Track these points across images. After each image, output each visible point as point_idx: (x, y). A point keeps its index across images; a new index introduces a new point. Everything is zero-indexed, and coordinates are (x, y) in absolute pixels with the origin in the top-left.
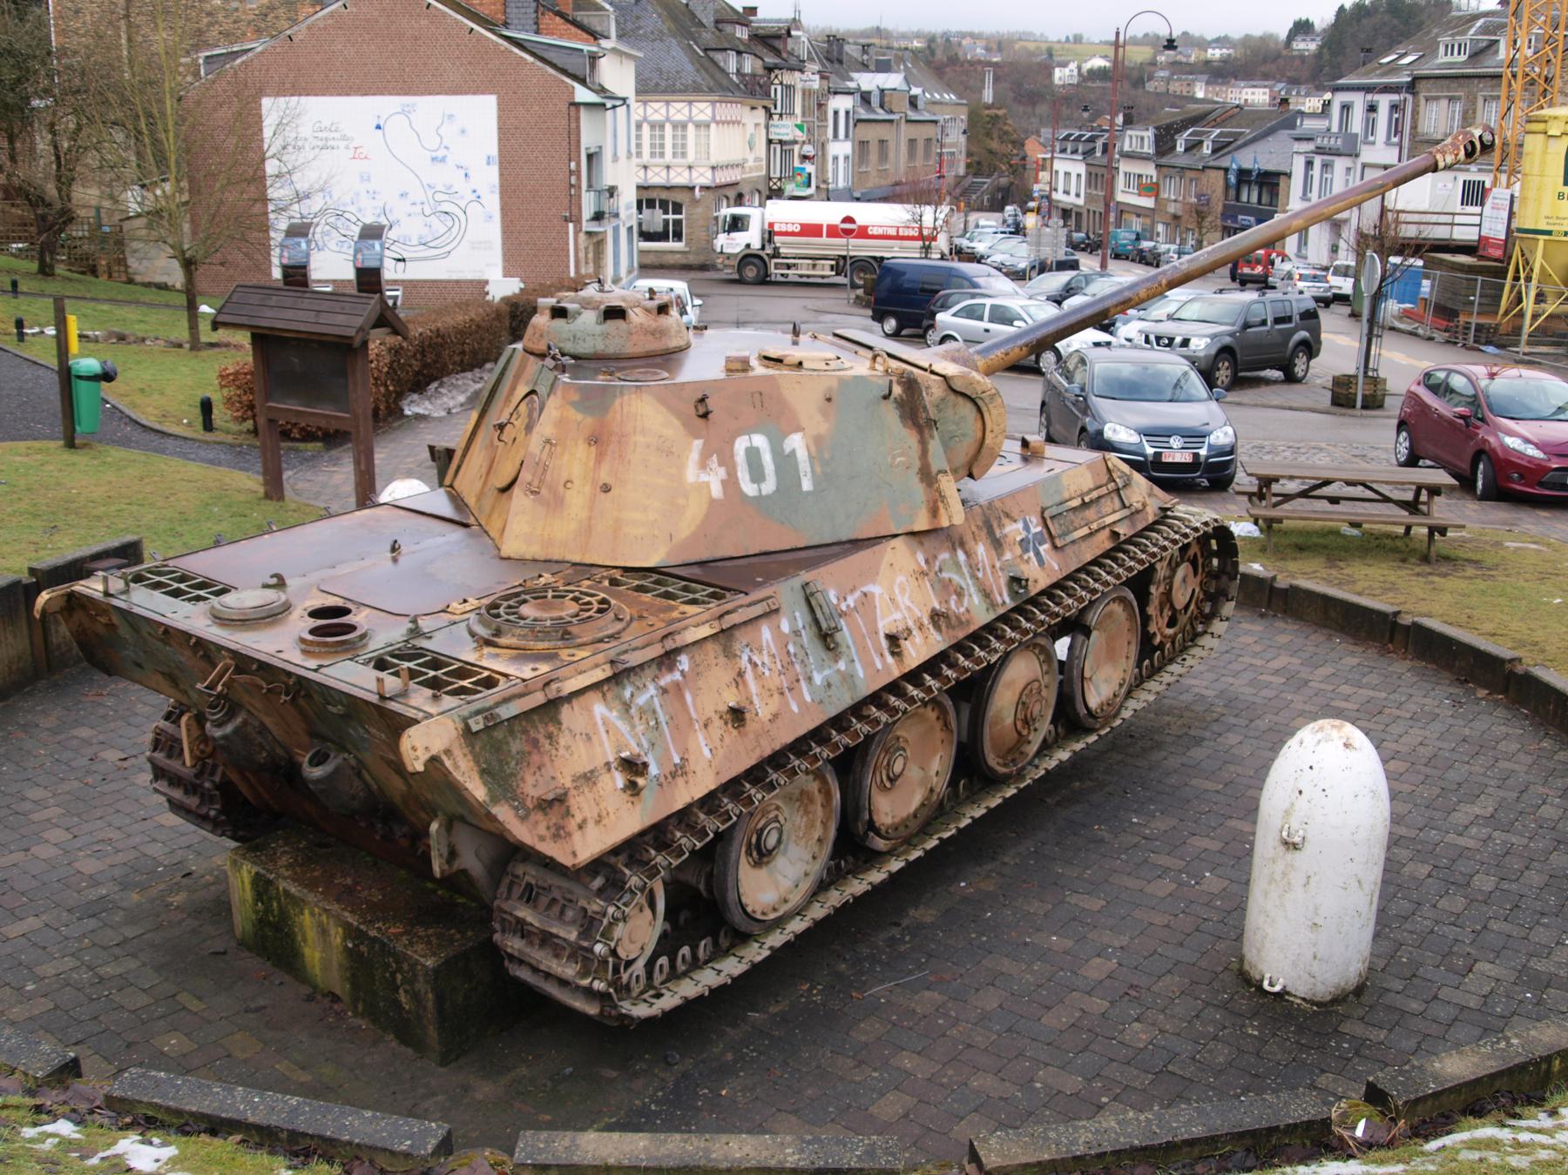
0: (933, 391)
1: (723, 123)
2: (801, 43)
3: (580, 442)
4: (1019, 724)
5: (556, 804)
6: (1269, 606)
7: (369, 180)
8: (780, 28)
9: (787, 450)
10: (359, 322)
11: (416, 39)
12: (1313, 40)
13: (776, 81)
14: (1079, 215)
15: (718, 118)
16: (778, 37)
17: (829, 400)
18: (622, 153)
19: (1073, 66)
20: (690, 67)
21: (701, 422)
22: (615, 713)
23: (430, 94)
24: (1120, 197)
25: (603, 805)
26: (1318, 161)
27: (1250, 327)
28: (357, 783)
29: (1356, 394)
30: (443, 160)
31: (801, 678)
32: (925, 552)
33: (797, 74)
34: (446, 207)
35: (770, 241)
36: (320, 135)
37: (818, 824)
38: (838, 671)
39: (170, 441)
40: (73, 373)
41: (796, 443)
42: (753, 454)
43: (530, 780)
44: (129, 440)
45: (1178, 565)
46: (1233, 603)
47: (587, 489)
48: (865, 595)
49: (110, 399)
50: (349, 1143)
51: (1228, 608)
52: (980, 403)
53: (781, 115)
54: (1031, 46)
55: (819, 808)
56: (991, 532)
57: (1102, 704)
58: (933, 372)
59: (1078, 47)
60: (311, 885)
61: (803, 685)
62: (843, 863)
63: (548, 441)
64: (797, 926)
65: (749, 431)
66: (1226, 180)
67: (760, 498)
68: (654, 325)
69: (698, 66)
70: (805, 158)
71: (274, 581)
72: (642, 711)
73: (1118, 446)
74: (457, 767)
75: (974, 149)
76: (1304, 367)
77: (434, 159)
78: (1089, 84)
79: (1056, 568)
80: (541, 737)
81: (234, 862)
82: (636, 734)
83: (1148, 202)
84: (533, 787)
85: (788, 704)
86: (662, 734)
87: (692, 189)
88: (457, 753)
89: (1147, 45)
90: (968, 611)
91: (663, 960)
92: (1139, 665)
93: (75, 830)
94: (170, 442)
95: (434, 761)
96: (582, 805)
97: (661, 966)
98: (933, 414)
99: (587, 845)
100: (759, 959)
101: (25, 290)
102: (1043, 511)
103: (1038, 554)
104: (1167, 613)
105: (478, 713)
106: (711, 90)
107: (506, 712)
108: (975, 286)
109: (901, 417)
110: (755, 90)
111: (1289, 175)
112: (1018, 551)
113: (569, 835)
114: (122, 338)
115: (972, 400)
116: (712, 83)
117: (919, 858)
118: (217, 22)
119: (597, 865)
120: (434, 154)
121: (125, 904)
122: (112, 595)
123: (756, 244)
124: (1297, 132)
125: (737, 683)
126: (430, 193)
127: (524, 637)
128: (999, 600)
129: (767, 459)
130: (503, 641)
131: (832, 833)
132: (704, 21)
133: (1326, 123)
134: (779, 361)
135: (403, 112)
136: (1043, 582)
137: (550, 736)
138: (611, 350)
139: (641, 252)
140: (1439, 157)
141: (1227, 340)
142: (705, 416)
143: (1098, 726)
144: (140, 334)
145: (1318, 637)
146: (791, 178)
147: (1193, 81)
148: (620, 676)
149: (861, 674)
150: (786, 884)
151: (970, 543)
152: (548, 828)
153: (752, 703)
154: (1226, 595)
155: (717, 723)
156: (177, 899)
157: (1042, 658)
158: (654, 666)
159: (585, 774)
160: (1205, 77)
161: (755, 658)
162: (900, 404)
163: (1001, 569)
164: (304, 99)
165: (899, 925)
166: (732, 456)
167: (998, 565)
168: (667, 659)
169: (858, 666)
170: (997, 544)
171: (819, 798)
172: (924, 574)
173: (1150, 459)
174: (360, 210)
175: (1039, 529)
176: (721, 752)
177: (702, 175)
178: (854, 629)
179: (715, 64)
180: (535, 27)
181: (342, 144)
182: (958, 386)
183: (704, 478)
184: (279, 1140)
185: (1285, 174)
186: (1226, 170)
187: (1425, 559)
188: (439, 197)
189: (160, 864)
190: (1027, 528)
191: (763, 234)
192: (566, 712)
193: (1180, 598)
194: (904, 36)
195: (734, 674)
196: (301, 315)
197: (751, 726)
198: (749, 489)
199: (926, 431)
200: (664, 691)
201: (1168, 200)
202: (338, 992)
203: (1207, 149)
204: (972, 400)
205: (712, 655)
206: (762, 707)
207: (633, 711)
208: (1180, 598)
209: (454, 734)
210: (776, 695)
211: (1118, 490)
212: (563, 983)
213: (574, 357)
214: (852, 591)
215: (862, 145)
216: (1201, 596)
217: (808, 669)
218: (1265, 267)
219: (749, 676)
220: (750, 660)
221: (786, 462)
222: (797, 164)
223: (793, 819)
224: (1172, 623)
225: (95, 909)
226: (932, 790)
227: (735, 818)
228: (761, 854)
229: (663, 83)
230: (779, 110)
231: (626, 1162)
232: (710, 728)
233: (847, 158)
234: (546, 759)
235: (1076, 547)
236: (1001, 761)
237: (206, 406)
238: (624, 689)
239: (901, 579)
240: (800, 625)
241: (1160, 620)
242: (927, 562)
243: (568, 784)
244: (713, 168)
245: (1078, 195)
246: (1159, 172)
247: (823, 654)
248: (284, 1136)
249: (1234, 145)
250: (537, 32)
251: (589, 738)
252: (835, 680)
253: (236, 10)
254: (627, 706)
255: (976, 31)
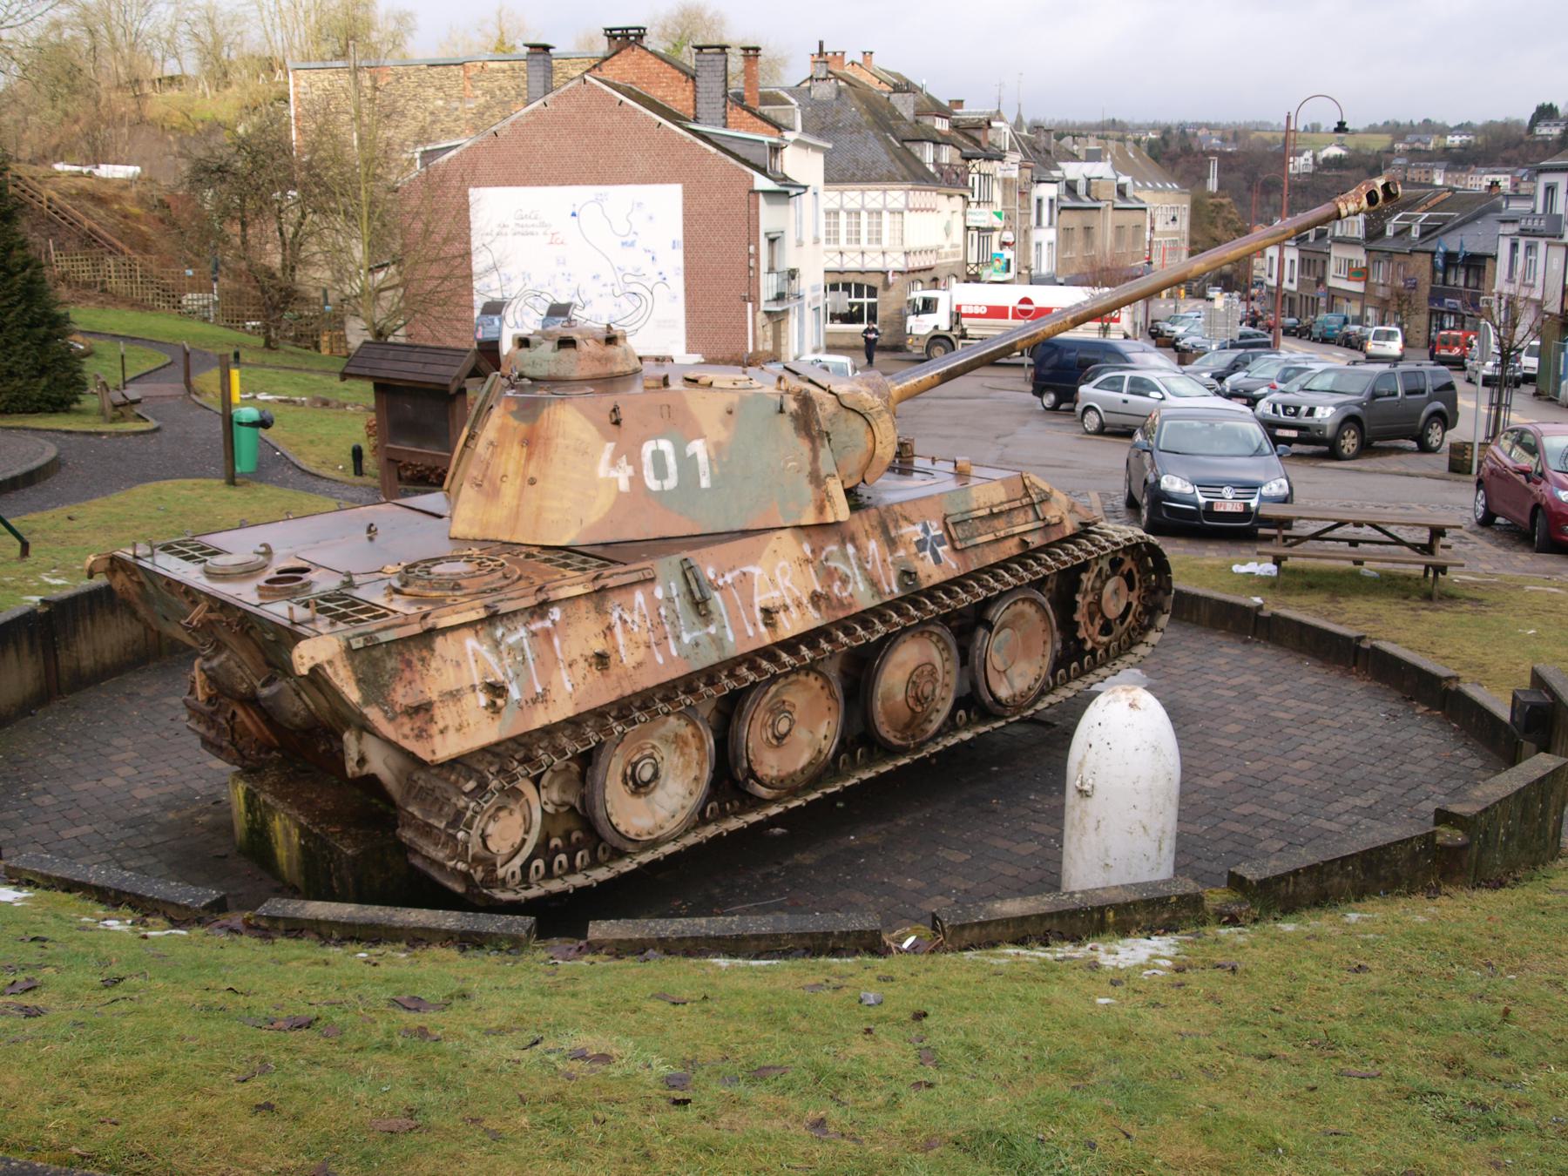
0: (826, 406)
1: (917, 210)
2: (1002, 133)
3: (516, 444)
4: (911, 701)
5: (422, 710)
6: (1254, 635)
7: (564, 263)
8: (980, 120)
9: (689, 453)
10: (456, 371)
11: (609, 133)
12: (1556, 125)
13: (974, 171)
14: (1291, 300)
15: (911, 206)
16: (978, 128)
17: (730, 412)
18: (808, 239)
19: (1308, 155)
20: (885, 158)
21: (616, 427)
22: (485, 647)
23: (621, 184)
24: (1331, 282)
25: (464, 717)
26: (1522, 242)
27: (1378, 397)
28: (298, 702)
29: (1471, 461)
30: (632, 244)
31: (669, 636)
32: (811, 544)
33: (996, 163)
34: (635, 288)
35: (957, 323)
36: (521, 222)
37: (694, 764)
38: (708, 634)
39: (324, 483)
40: (235, 419)
41: (698, 448)
42: (658, 457)
43: (400, 690)
44: (288, 481)
45: (1108, 577)
46: (1168, 616)
47: (519, 481)
48: (744, 574)
49: (280, 448)
50: (151, 898)
51: (1163, 620)
52: (868, 417)
53: (978, 203)
54: (1267, 136)
55: (694, 751)
56: (885, 531)
57: (1015, 695)
58: (831, 392)
59: (1315, 136)
60: (282, 798)
61: (671, 642)
62: (728, 806)
63: (491, 443)
64: (669, 849)
65: (656, 436)
66: (1433, 263)
67: (661, 493)
68: (601, 353)
69: (893, 156)
70: (1004, 244)
71: (263, 549)
72: (511, 648)
73: (1175, 496)
74: (336, 674)
75: (1197, 237)
76: (1439, 437)
77: (623, 244)
78: (1325, 173)
79: (954, 566)
80: (415, 661)
81: (234, 780)
82: (503, 666)
83: (1357, 287)
84: (402, 696)
85: (653, 656)
86: (528, 668)
87: (885, 273)
88: (339, 664)
89: (1387, 132)
90: (851, 595)
91: (539, 862)
92: (1053, 674)
93: (141, 769)
94: (322, 485)
95: (314, 670)
96: (445, 715)
97: (537, 868)
98: (825, 426)
99: (445, 747)
100: (626, 869)
101: (248, 361)
102: (946, 517)
103: (935, 554)
104: (1098, 622)
105: (360, 635)
106: (905, 180)
107: (384, 637)
108: (1128, 361)
109: (795, 428)
110: (950, 181)
111: (1495, 258)
112: (914, 549)
113: (431, 736)
114: (326, 403)
115: (862, 415)
116: (906, 173)
117: (800, 806)
118: (439, 121)
119: (454, 763)
120: (624, 240)
121: (161, 820)
122: (138, 558)
123: (944, 326)
124: (1504, 214)
125: (605, 636)
126: (620, 275)
127: (423, 587)
128: (887, 589)
129: (671, 460)
130: (407, 590)
131: (707, 774)
132: (905, 114)
133: (1531, 205)
134: (695, 381)
135: (596, 201)
136: (938, 577)
137: (423, 660)
138: (562, 373)
139: (828, 334)
140: (1341, 205)
141: (1356, 410)
142: (617, 423)
143: (1008, 714)
144: (342, 400)
145: (1291, 661)
146: (988, 264)
147: (1432, 168)
148: (493, 618)
149: (731, 638)
150: (663, 814)
151: (862, 539)
152: (412, 729)
153: (617, 651)
154: (1162, 609)
155: (582, 664)
156: (202, 819)
157: (941, 645)
158: (527, 614)
159: (451, 692)
160: (1445, 164)
161: (626, 616)
162: (795, 417)
163: (893, 563)
164: (482, 190)
165: (780, 864)
166: (639, 457)
167: (889, 559)
168: (541, 609)
169: (729, 632)
170: (892, 543)
171: (693, 742)
172: (807, 561)
173: (1203, 508)
174: (556, 291)
175: (939, 532)
176: (582, 688)
177: (894, 260)
178: (728, 601)
179: (912, 155)
180: (723, 121)
181: (541, 230)
182: (847, 402)
183: (614, 474)
184: (109, 897)
185: (1491, 257)
186: (1433, 253)
187: (1428, 597)
188: (628, 279)
189: (198, 794)
190: (926, 530)
191: (951, 316)
192: (439, 643)
193: (1113, 608)
194: (1139, 128)
195: (603, 627)
196: (411, 367)
197: (614, 670)
198: (653, 484)
199: (818, 441)
200: (534, 634)
201: (1377, 284)
202: (297, 884)
203: (1415, 233)
204: (862, 415)
205: (583, 609)
206: (627, 656)
207: (502, 647)
208: (1113, 608)
209: (337, 649)
210: (643, 649)
211: (1033, 505)
212: (433, 862)
213: (532, 379)
214: (731, 570)
215: (1067, 231)
216: (1140, 609)
217: (677, 630)
218: (1463, 348)
219: (618, 630)
220: (621, 617)
221: (687, 465)
222: (996, 249)
223: (670, 760)
224: (1106, 629)
225: (133, 823)
226: (820, 751)
227: (593, 744)
228: (635, 782)
229: (859, 174)
230: (976, 198)
231: (331, 919)
232: (574, 667)
233: (1050, 244)
234: (417, 677)
235: (979, 551)
236: (899, 735)
237: (357, 454)
238: (496, 628)
239: (781, 564)
240: (674, 593)
241: (1090, 627)
242: (813, 551)
243: (435, 697)
244: (906, 253)
245: (1291, 281)
246: (1368, 258)
247: (694, 619)
248: (112, 894)
249: (1442, 229)
250: (725, 126)
251: (458, 664)
252: (705, 641)
253: (456, 109)
254: (497, 644)
255: (1213, 122)
